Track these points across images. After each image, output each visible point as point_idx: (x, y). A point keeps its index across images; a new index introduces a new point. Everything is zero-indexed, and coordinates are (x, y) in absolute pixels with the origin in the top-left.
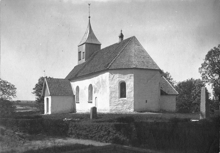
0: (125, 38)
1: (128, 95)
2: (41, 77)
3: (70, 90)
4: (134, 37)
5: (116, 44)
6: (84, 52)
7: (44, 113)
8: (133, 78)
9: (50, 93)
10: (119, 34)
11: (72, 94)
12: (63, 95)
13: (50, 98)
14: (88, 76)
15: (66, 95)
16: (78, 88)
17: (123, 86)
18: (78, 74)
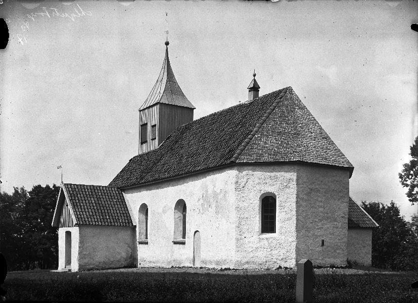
0: (261, 93)
1: (282, 227)
2: (36, 184)
3: (124, 212)
4: (288, 90)
5: (240, 107)
6: (155, 125)
7: (57, 268)
8: (293, 185)
9: (78, 219)
10: (249, 83)
11: (129, 223)
12: (108, 225)
13: (75, 232)
14: (159, 183)
15: (115, 225)
16: (144, 209)
17: (268, 205)
18: (143, 173)
